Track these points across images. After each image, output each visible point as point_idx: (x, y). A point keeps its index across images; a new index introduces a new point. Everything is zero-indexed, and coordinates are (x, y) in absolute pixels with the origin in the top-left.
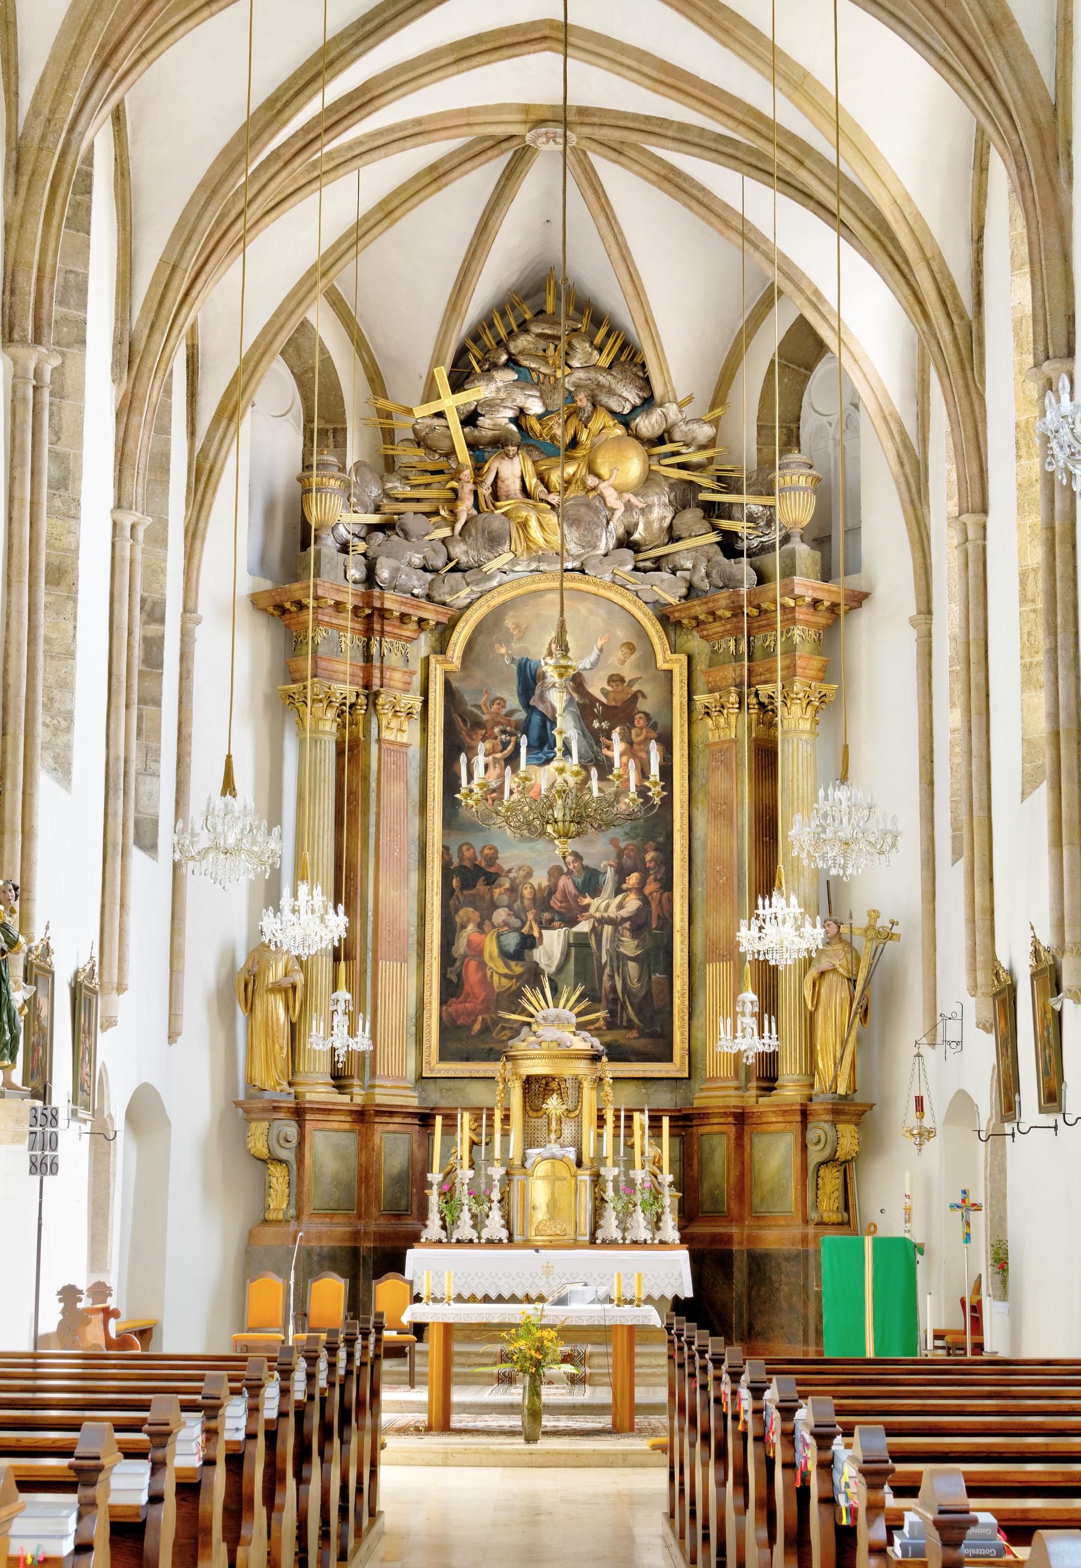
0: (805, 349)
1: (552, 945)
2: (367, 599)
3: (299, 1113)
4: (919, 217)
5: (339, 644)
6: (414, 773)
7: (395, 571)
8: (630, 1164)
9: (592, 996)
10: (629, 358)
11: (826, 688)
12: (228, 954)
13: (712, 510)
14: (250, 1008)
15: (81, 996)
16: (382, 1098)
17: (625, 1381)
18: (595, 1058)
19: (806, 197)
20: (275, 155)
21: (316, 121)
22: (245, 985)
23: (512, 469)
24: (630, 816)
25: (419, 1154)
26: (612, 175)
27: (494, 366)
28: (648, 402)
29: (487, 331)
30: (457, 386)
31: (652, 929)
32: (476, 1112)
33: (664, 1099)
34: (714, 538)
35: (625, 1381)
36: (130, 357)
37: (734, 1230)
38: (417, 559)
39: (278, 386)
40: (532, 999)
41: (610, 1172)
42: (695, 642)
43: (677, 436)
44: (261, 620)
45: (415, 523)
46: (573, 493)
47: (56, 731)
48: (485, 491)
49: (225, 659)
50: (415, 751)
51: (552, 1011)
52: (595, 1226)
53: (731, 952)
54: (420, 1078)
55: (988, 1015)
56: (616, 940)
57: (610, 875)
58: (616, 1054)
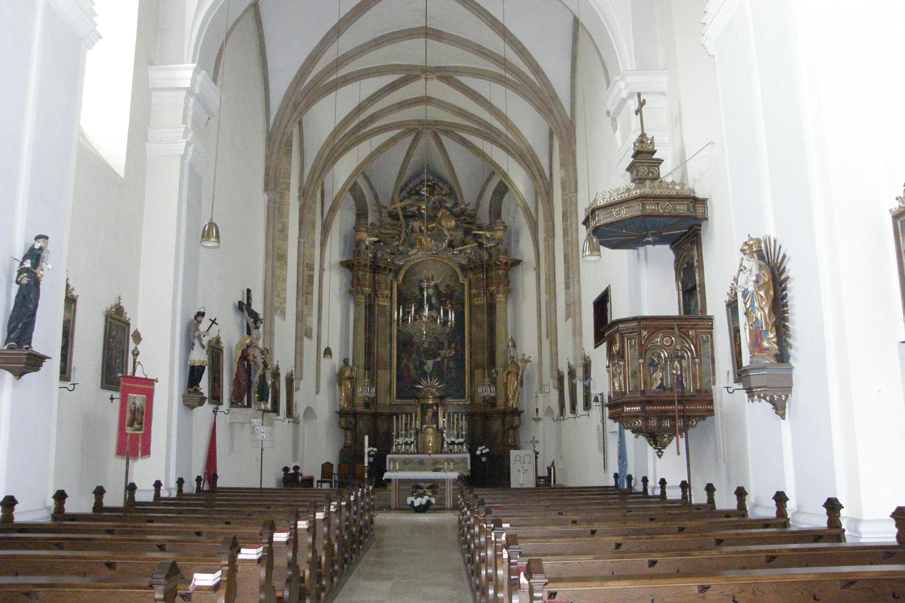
0: (503, 189)
2: (373, 263)
7: (382, 255)
15: (290, 381)
24: (447, 334)
26: (444, 139)
28: (456, 205)
34: (476, 244)
36: (304, 193)
38: (389, 251)
39: (349, 202)
42: (471, 275)
46: (436, 231)
47: (281, 303)
49: (333, 283)
50: (388, 308)
57: (446, 344)
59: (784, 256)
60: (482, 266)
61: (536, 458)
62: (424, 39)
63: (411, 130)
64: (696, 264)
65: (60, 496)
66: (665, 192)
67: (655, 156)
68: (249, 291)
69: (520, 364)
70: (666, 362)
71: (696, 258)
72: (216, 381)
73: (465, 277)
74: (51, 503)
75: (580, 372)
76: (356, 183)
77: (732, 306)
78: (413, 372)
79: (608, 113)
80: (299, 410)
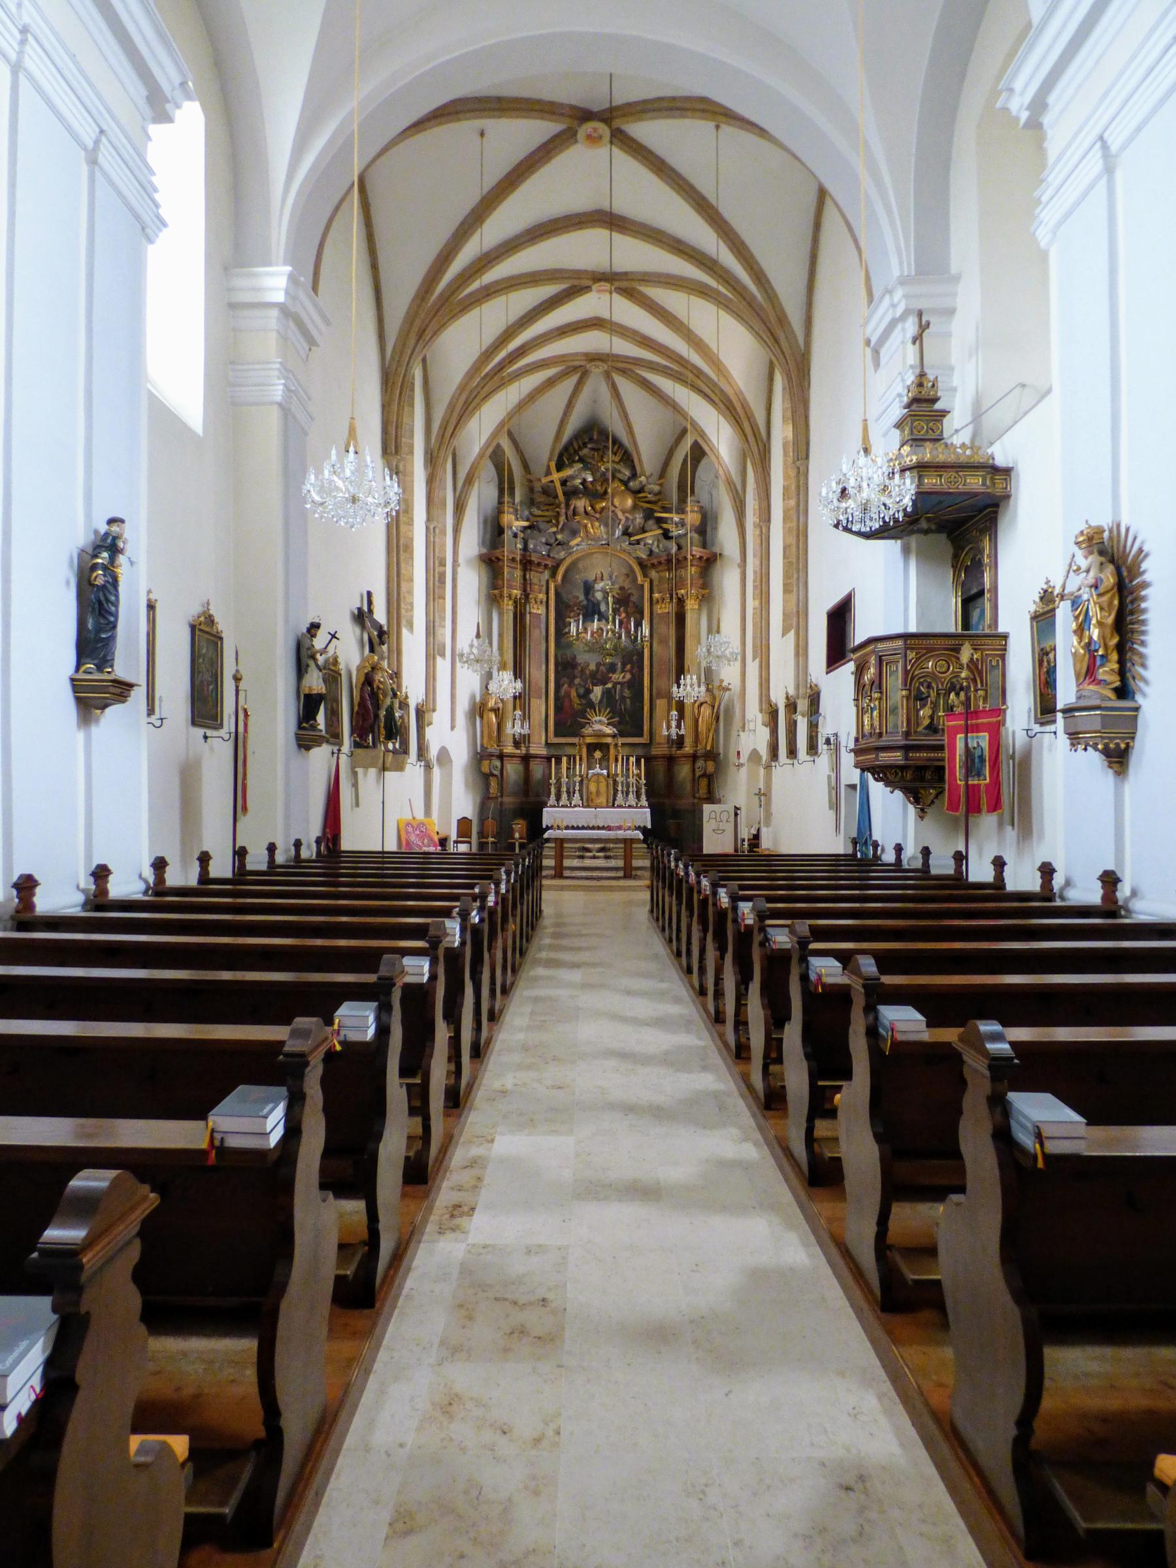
0: (698, 453)
1: (597, 692)
2: (523, 556)
3: (501, 757)
4: (745, 399)
5: (512, 574)
6: (543, 626)
7: (535, 546)
8: (628, 776)
9: (614, 713)
10: (627, 458)
11: (704, 592)
12: (473, 697)
13: (660, 521)
14: (482, 717)
15: (420, 713)
16: (533, 751)
17: (628, 857)
18: (614, 736)
19: (700, 391)
20: (487, 374)
21: (504, 359)
22: (479, 709)
23: (581, 503)
25: (547, 772)
26: (622, 382)
27: (574, 462)
29: (689, 557)
30: (559, 469)
31: (635, 685)
32: (569, 757)
33: (640, 751)
34: (660, 531)
35: (628, 857)
36: (432, 460)
37: (666, 801)
38: (544, 540)
40: (590, 714)
41: (620, 779)
42: (653, 574)
43: (646, 489)
44: (483, 566)
45: (542, 526)
47: (407, 610)
48: (570, 512)
49: (469, 583)
50: (543, 618)
51: (598, 718)
52: (614, 799)
53: (669, 696)
54: (547, 743)
55: (767, 719)
56: (622, 691)
58: (622, 734)
59: (1140, 550)
60: (669, 561)
61: (736, 814)
62: (608, 232)
63: (575, 369)
64: (986, 560)
65: (160, 865)
66: (952, 459)
67: (938, 406)
68: (369, 594)
69: (716, 692)
70: (938, 694)
71: (987, 552)
72: (333, 716)
73: (645, 575)
74: (149, 874)
75: (803, 705)
76: (498, 446)
77: (1043, 620)
78: (576, 701)
79: (868, 342)
80: (433, 752)
